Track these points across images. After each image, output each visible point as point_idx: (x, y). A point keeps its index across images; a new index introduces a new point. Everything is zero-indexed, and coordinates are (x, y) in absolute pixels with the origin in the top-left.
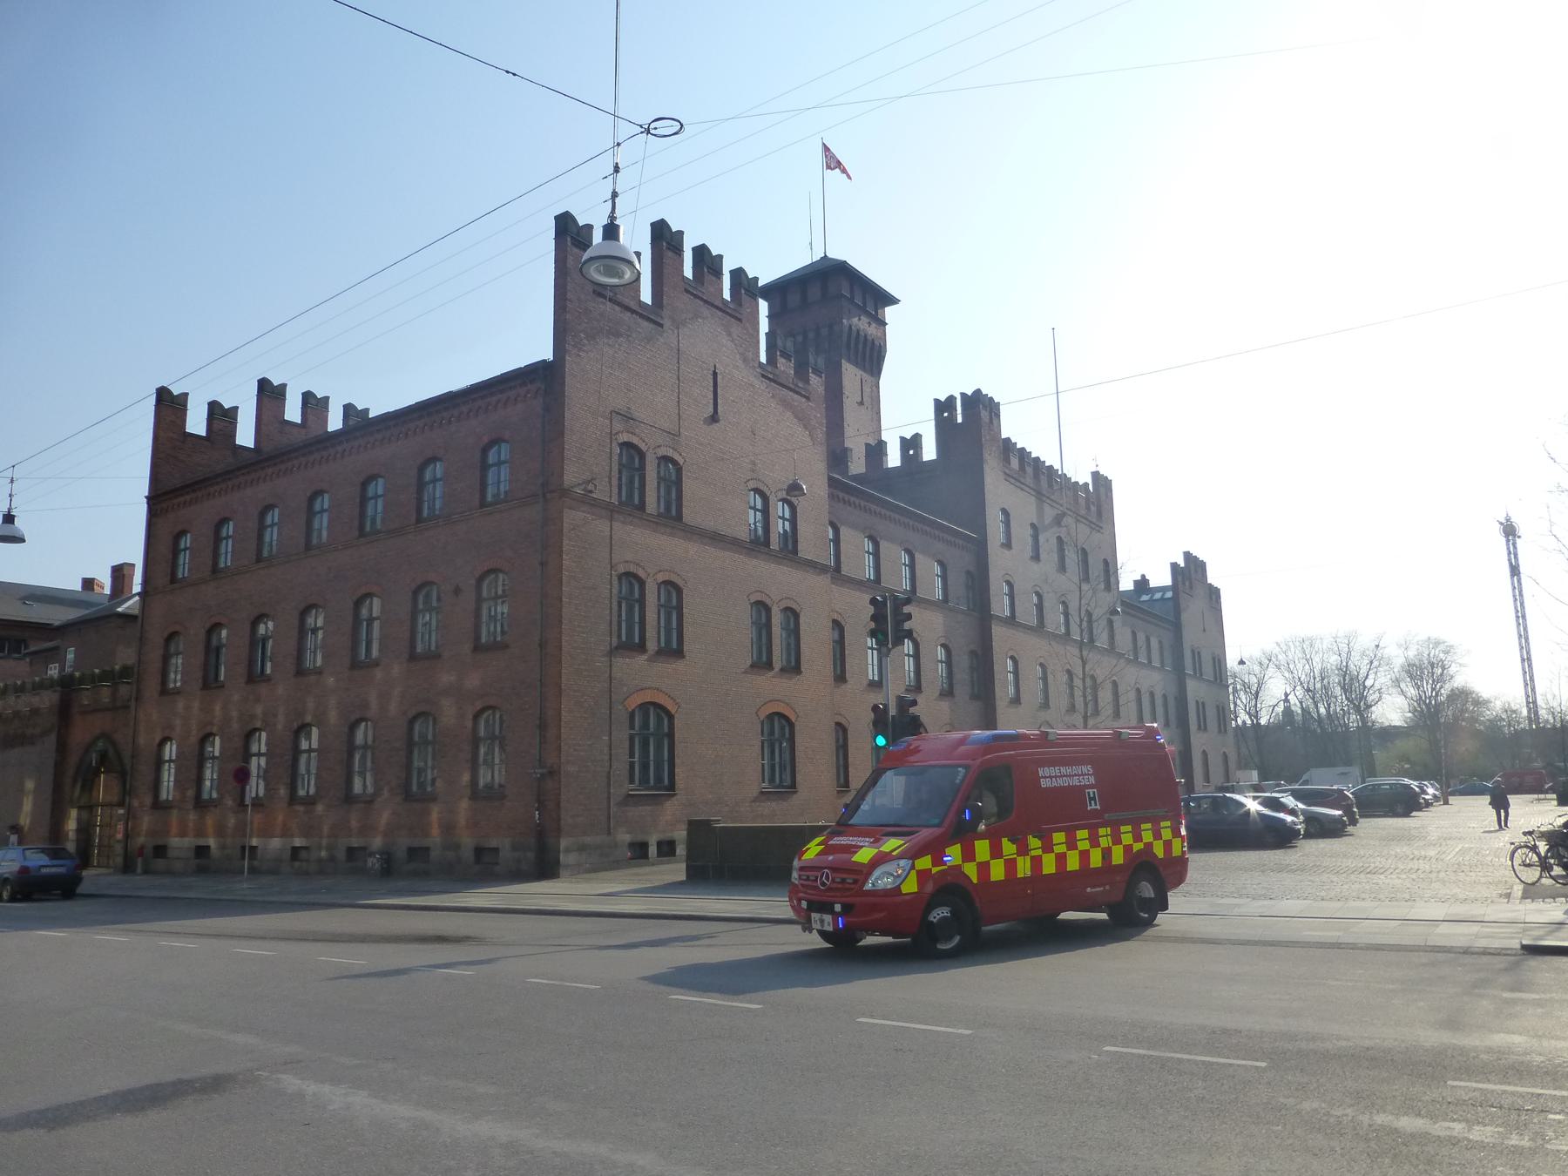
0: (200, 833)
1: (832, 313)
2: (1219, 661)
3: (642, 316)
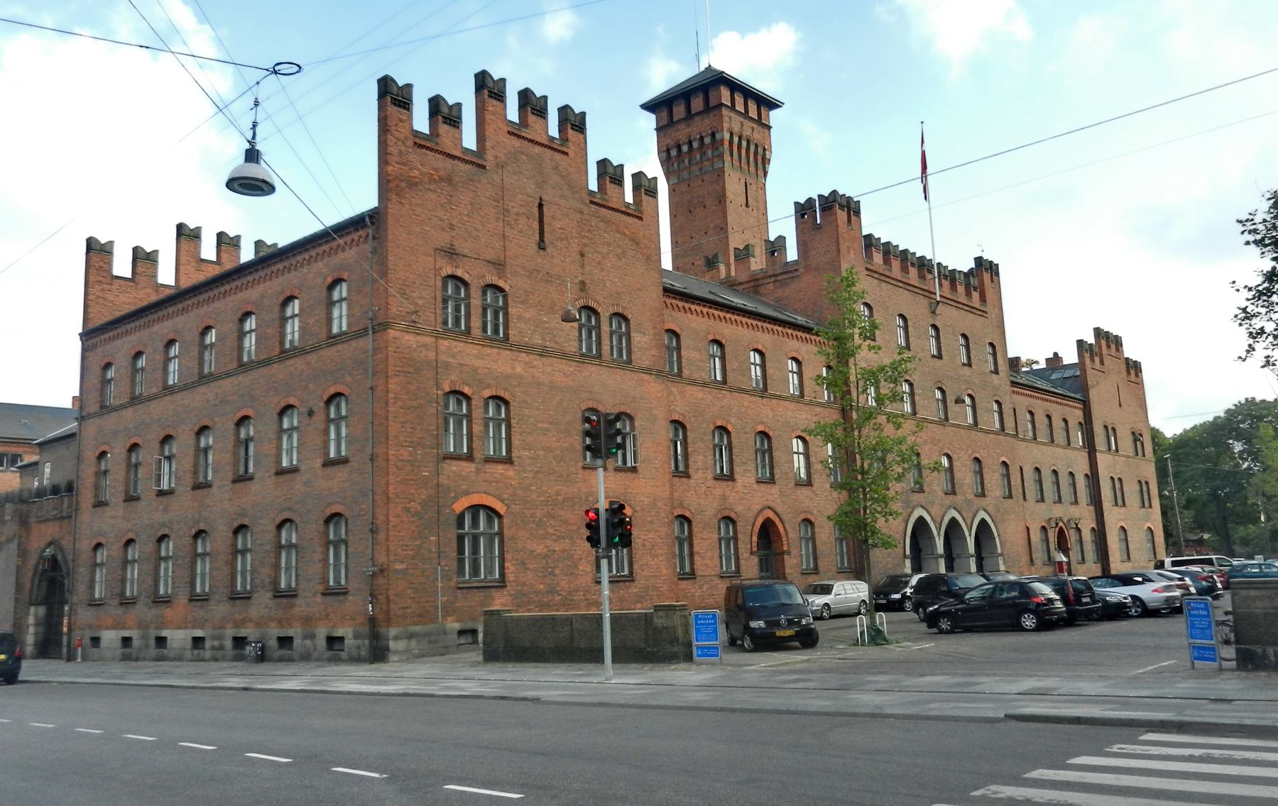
1: (709, 120)
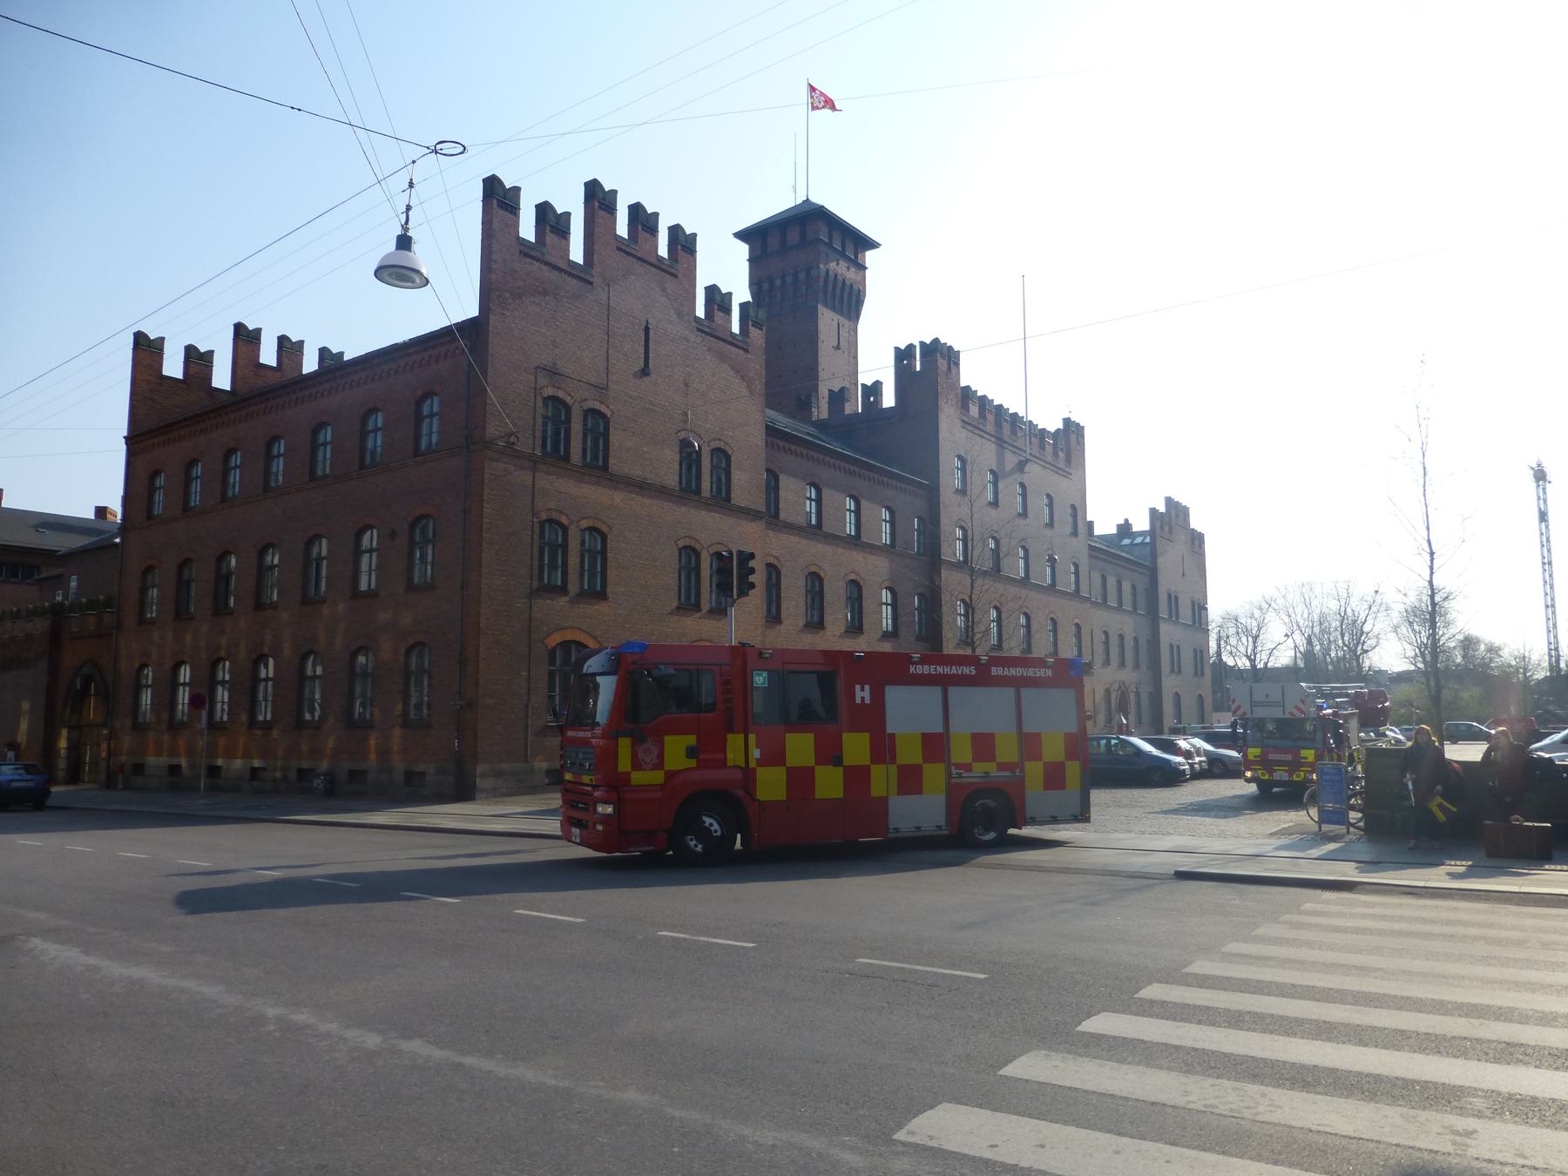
0: (173, 753)
1: (809, 255)
2: (1200, 608)
3: (570, 274)
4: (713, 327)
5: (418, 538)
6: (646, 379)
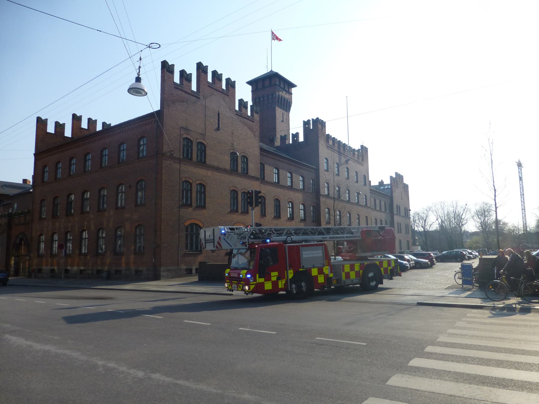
1: (273, 89)
2: (407, 210)
3: (192, 95)
4: (241, 114)
5: (139, 188)
6: (219, 132)
